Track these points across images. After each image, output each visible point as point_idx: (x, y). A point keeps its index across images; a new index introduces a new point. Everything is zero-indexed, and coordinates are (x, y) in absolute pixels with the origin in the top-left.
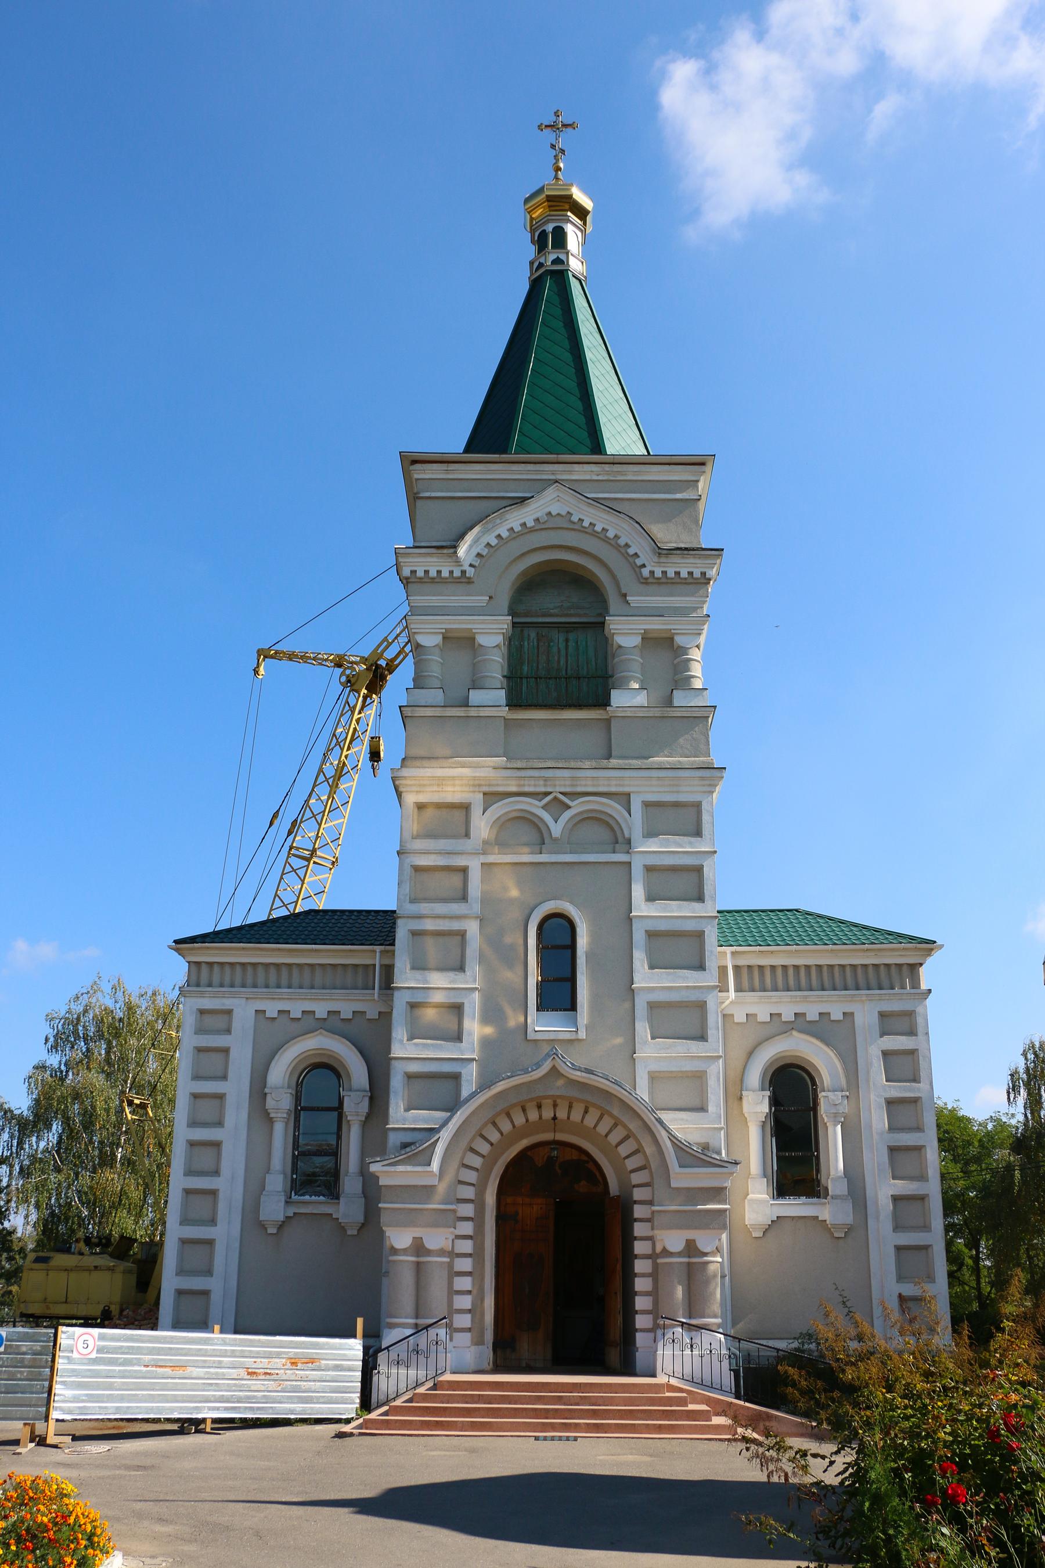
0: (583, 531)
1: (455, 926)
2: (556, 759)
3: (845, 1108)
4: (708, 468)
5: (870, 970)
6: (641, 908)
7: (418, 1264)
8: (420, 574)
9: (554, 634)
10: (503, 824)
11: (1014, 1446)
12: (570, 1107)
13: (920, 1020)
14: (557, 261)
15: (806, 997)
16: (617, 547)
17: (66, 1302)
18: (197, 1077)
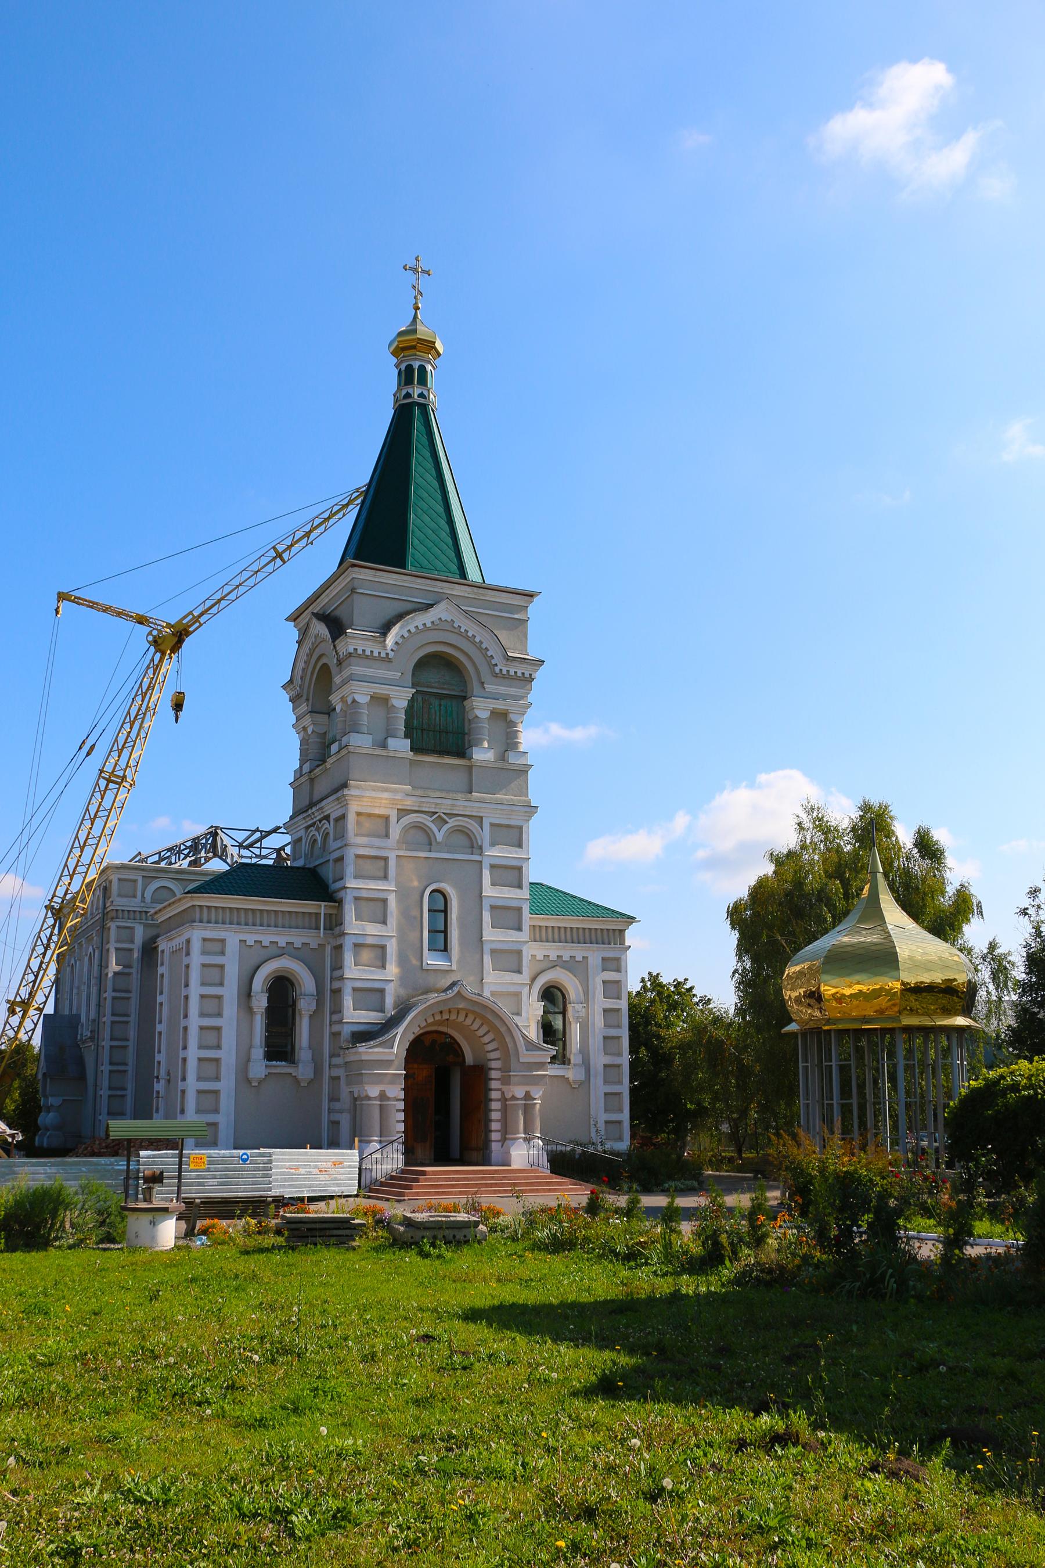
0: (460, 634)
1: (381, 895)
2: (442, 790)
3: (583, 1013)
4: (536, 599)
5: (599, 932)
6: (488, 891)
7: (381, 1105)
8: (360, 652)
10: (406, 829)
11: (462, 1217)
12: (458, 1013)
13: (623, 964)
14: (421, 395)
15: (564, 946)
16: (474, 643)
18: (203, 984)
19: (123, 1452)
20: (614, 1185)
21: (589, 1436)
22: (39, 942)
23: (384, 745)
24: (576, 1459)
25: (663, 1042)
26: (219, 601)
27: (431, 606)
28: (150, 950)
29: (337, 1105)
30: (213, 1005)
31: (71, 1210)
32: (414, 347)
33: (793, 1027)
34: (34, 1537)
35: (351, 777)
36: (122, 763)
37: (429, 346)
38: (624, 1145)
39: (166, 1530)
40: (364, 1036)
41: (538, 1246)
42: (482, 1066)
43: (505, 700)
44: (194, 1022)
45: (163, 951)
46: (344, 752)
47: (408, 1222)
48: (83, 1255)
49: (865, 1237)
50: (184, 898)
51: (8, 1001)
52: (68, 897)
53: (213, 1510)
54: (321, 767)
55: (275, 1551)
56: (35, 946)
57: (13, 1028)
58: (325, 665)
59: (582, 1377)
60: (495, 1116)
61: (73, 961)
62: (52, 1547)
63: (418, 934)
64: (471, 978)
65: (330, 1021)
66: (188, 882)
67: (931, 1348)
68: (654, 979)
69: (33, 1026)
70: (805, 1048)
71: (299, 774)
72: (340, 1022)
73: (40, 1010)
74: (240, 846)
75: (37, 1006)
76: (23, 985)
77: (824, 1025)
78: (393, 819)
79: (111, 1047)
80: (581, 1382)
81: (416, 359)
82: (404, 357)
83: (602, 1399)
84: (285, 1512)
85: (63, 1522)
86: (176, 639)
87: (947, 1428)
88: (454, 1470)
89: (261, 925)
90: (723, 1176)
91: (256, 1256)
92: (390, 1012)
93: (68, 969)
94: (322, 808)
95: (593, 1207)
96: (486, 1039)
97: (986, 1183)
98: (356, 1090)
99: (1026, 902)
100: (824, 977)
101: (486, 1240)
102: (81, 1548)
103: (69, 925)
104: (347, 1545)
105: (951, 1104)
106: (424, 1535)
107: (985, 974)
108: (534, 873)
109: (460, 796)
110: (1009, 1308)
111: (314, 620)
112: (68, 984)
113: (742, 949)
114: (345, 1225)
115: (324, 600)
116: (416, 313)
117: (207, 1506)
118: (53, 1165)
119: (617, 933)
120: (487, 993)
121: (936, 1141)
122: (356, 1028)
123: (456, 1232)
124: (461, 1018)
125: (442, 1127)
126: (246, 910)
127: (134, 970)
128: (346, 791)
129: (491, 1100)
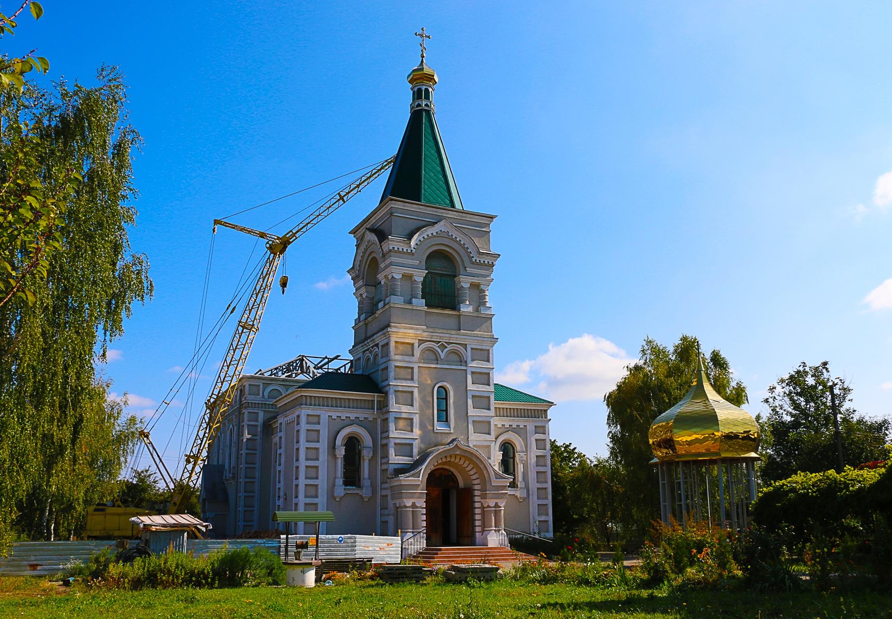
0: (452, 239)
1: (410, 389)
3: (525, 458)
5: (533, 411)
6: (471, 386)
7: (413, 511)
10: (423, 351)
12: (456, 458)
14: (426, 105)
16: (460, 244)
17: (119, 530)
22: (204, 421)
23: (410, 303)
27: (436, 223)
29: (386, 512)
30: (313, 454)
35: (392, 321)
36: (252, 317)
37: (430, 78)
42: (470, 488)
43: (478, 277)
44: (303, 463)
46: (387, 307)
50: (296, 391)
56: (202, 423)
57: (188, 471)
58: (374, 258)
60: (477, 517)
63: (431, 411)
64: (462, 437)
65: (381, 463)
69: (189, 475)
71: (358, 321)
72: (387, 463)
75: (202, 458)
78: (416, 345)
79: (246, 482)
81: (423, 85)
86: (283, 246)
89: (341, 407)
94: (374, 340)
98: (397, 502)
99: (768, 395)
100: (675, 431)
108: (498, 378)
109: (453, 332)
111: (368, 232)
115: (373, 220)
116: (422, 60)
119: (543, 412)
122: (396, 467)
126: (332, 398)
127: (258, 438)
129: (475, 508)
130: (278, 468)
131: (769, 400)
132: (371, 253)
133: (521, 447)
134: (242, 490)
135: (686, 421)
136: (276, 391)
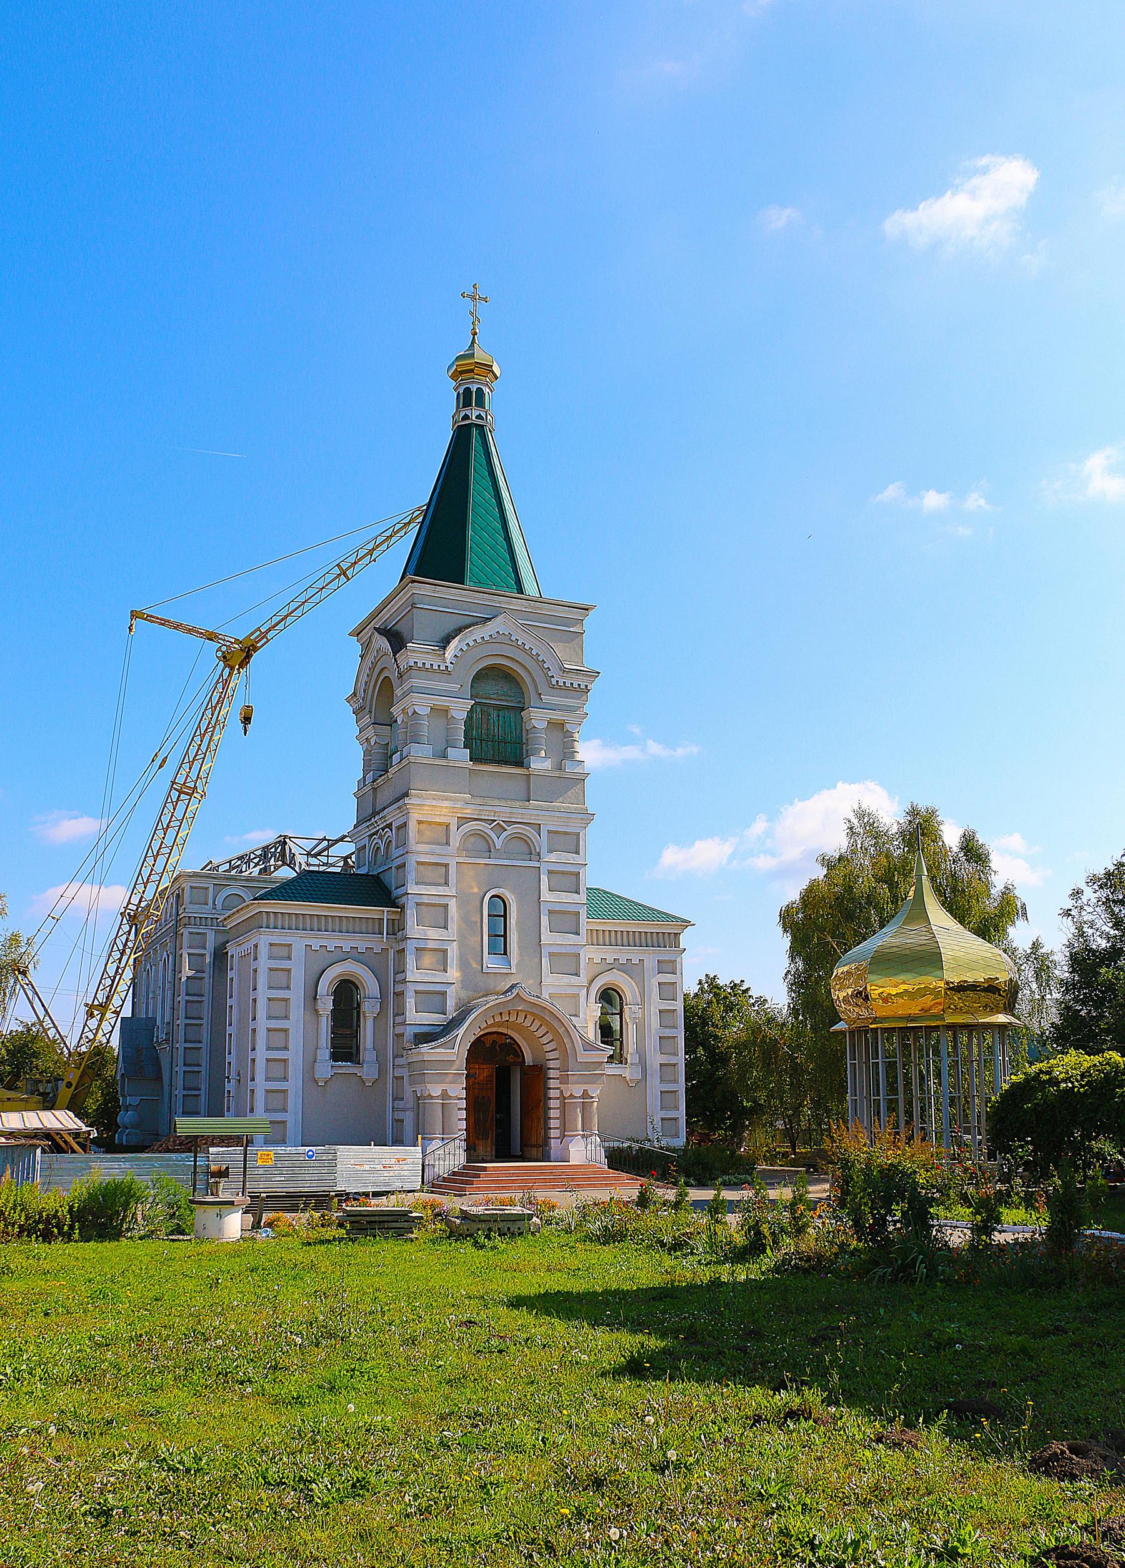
1: (442, 901)
6: (546, 895)
9: (491, 711)
11: (517, 1210)
14: (479, 417)
16: (531, 655)
19: (164, 1425)
20: (664, 1177)
21: (611, 1413)
23: (444, 756)
24: (596, 1434)
25: (719, 1042)
26: (286, 617)
27: (490, 619)
28: (220, 956)
29: (401, 1104)
31: (142, 1203)
32: (472, 371)
33: (840, 1026)
34: (70, 1498)
38: (680, 1142)
39: (194, 1495)
40: (426, 1037)
41: (589, 1238)
45: (232, 956)
46: (405, 762)
47: (465, 1216)
48: (152, 1245)
49: (899, 1225)
51: (86, 1005)
52: (143, 904)
53: (240, 1479)
54: (383, 777)
55: (294, 1516)
56: (112, 951)
59: (613, 1359)
60: (553, 1113)
61: (148, 967)
62: (87, 1507)
64: (531, 982)
66: (257, 890)
67: (951, 1328)
68: (712, 981)
70: (853, 1046)
72: (404, 1023)
73: (117, 1013)
74: (308, 854)
75: (114, 1009)
76: (100, 989)
77: (871, 1024)
78: (453, 828)
80: (611, 1364)
82: (461, 380)
83: (629, 1380)
84: (308, 1481)
85: (99, 1485)
87: (953, 1402)
88: (477, 1445)
90: (777, 1170)
91: (318, 1247)
92: (451, 1013)
93: (145, 974)
94: (384, 817)
95: (643, 1201)
96: (545, 1040)
97: (1026, 1173)
98: (418, 1088)
99: (1069, 904)
100: (871, 977)
101: (539, 1232)
102: (112, 1510)
103: (143, 931)
104: (363, 1511)
105: (993, 1098)
106: (435, 1503)
107: (1029, 973)
108: (591, 879)
110: (1031, 1290)
112: (144, 988)
113: (794, 952)
114: (406, 1218)
115: (385, 614)
116: (474, 337)
117: (236, 1475)
118: (126, 1160)
120: (545, 995)
121: (980, 1134)
122: (418, 1030)
123: (510, 1224)
124: (520, 1020)
125: (504, 1124)
128: (407, 800)
130: (229, 1030)
131: (1072, 913)
132: (383, 669)
133: (634, 996)
134: (181, 1062)
135: (886, 962)
136: (237, 897)
